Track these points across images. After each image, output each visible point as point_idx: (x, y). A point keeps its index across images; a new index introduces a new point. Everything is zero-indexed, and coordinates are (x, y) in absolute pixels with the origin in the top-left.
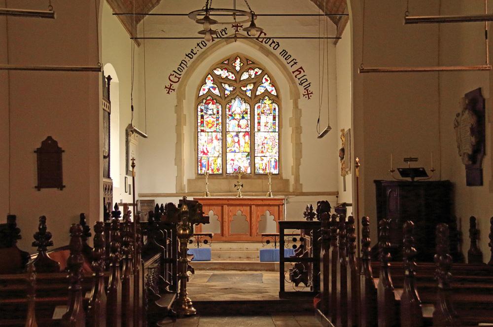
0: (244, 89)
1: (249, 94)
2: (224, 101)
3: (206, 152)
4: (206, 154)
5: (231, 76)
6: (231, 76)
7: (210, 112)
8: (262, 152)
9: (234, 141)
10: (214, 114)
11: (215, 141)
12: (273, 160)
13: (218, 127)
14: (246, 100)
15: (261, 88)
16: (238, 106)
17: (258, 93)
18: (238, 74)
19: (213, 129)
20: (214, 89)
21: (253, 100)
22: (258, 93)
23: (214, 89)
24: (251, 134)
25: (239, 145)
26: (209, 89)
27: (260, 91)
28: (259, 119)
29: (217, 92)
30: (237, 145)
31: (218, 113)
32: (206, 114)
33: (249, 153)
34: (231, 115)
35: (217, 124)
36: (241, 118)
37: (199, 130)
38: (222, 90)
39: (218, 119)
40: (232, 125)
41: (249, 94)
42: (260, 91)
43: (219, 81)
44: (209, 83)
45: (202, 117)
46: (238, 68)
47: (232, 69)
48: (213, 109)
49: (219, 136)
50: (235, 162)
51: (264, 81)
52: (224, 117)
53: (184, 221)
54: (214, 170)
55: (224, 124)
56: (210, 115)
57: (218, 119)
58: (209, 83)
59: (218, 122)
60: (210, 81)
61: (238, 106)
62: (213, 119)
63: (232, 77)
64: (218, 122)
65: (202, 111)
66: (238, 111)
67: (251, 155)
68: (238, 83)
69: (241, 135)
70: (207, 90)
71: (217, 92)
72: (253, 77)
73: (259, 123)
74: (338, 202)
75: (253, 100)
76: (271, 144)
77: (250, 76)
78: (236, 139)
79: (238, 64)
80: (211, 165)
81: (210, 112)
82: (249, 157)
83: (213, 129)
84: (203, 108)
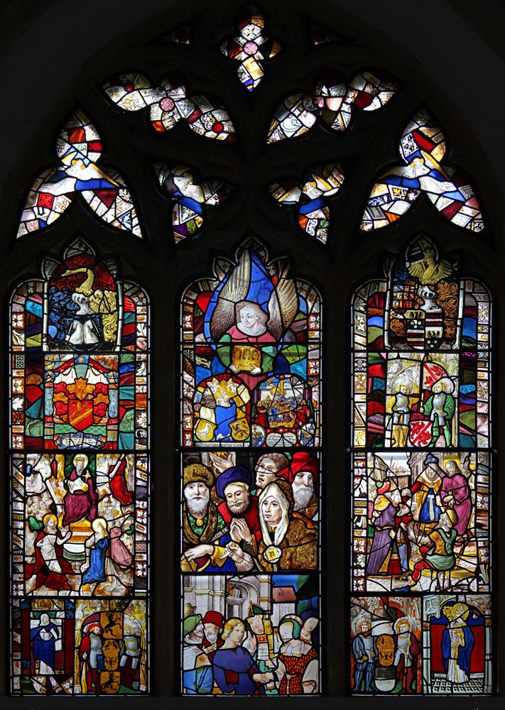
0: (401, 604)
1: (314, 223)
2: (166, 271)
3: (56, 567)
4: (57, 582)
5: (212, 125)
6: (212, 125)
7: (81, 334)
8: (395, 570)
9: (217, 505)
10: (105, 347)
11: (110, 508)
12: (458, 614)
13: (127, 426)
14: (286, 253)
15: (395, 190)
16: (247, 305)
17: (373, 222)
18: (254, 110)
19: (101, 432)
20: (109, 198)
21: (347, 267)
22: (373, 222)
23: (109, 198)
24: (332, 465)
25: (255, 528)
26: (75, 196)
27: (388, 204)
28: (378, 371)
29: (119, 212)
30: (240, 530)
31: (129, 337)
32: (58, 344)
33: (312, 574)
34: (211, 355)
35: (123, 406)
36: (268, 365)
37: (18, 442)
38: (158, 205)
39: (125, 377)
40: (211, 411)
41: (314, 223)
42: (388, 204)
43: (137, 156)
44: (80, 166)
45: (34, 360)
46: (252, 71)
47: (214, 83)
48: (97, 319)
49: (138, 474)
50: (233, 636)
51: (407, 145)
52: (167, 359)
53: (429, 347)
54: (105, 677)
55: (166, 406)
56: (83, 348)
57: (125, 377)
58: (80, 166)
59: (127, 394)
60: (82, 147)
61: (247, 305)
62: (94, 378)
63: (217, 127)
64: (127, 394)
65: (32, 326)
66: (250, 322)
67: (325, 588)
68: (249, 171)
69: (267, 467)
70: (61, 204)
71: (119, 212)
72: (343, 120)
73: (376, 398)
74: (107, 209)
75: (347, 267)
76: (446, 520)
77: (325, 117)
78: (235, 493)
79: (252, 49)
80: (86, 647)
81: (81, 334)
82: (317, 602)
83: (101, 432)
84: (40, 308)
